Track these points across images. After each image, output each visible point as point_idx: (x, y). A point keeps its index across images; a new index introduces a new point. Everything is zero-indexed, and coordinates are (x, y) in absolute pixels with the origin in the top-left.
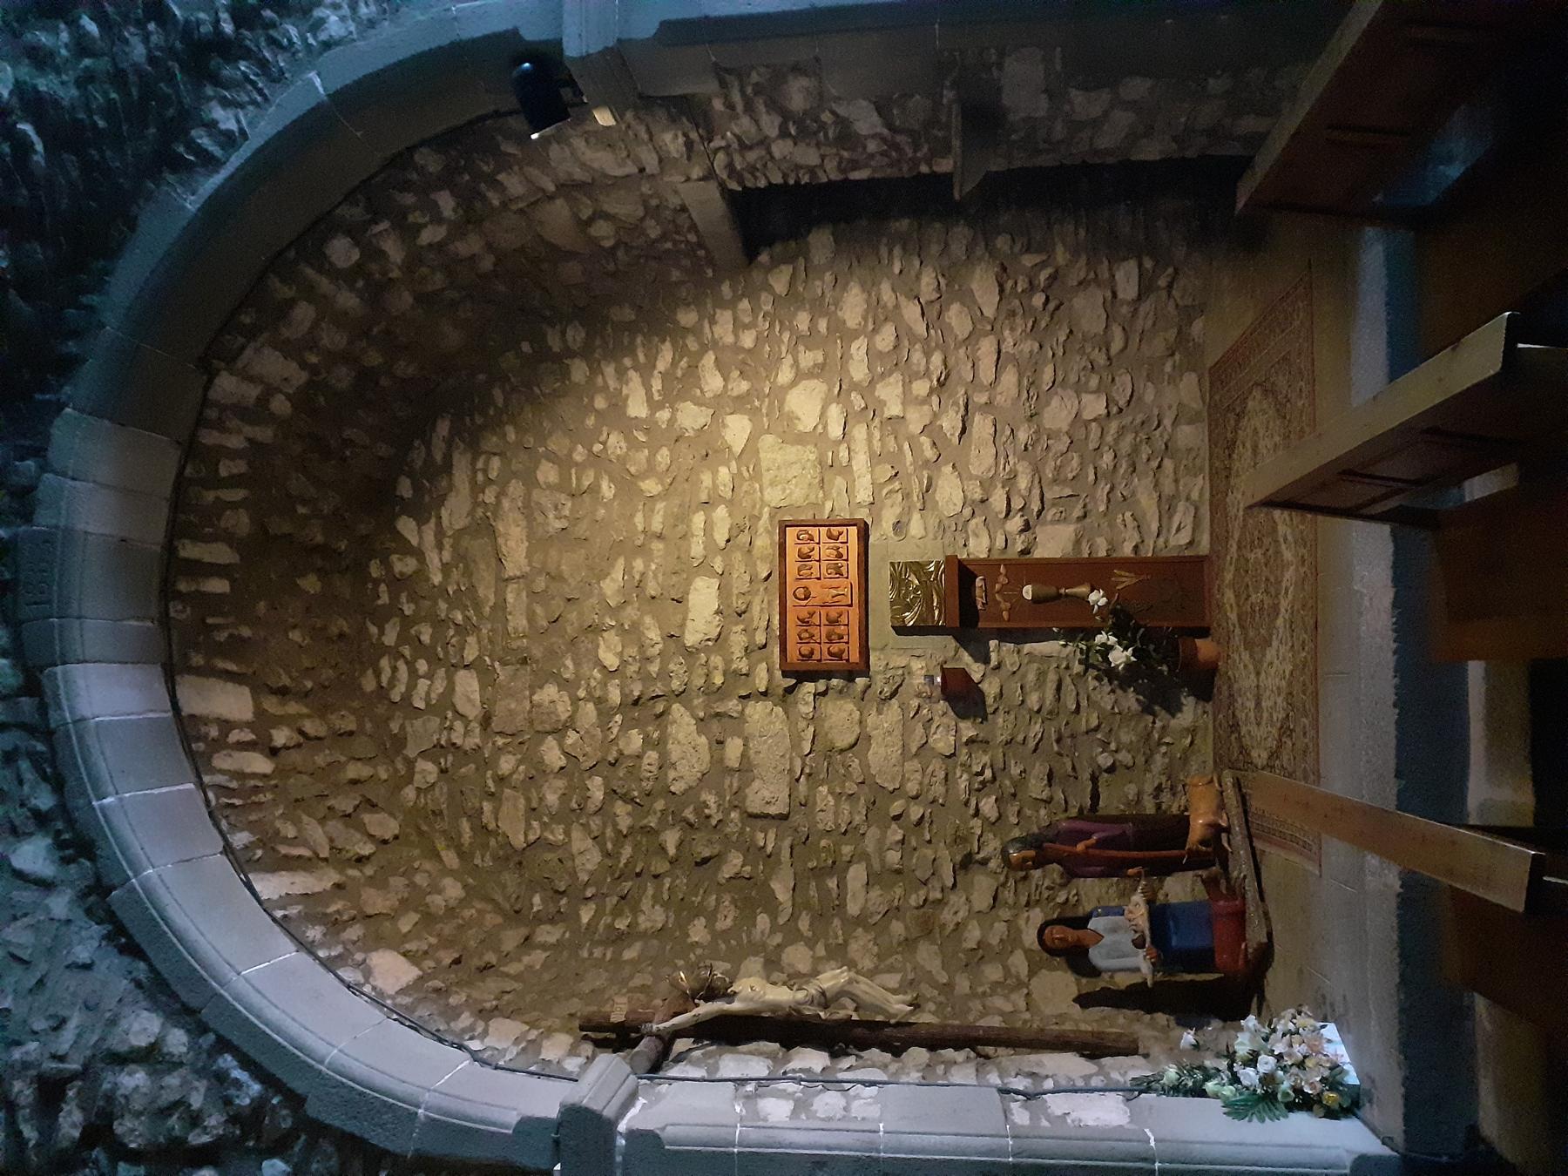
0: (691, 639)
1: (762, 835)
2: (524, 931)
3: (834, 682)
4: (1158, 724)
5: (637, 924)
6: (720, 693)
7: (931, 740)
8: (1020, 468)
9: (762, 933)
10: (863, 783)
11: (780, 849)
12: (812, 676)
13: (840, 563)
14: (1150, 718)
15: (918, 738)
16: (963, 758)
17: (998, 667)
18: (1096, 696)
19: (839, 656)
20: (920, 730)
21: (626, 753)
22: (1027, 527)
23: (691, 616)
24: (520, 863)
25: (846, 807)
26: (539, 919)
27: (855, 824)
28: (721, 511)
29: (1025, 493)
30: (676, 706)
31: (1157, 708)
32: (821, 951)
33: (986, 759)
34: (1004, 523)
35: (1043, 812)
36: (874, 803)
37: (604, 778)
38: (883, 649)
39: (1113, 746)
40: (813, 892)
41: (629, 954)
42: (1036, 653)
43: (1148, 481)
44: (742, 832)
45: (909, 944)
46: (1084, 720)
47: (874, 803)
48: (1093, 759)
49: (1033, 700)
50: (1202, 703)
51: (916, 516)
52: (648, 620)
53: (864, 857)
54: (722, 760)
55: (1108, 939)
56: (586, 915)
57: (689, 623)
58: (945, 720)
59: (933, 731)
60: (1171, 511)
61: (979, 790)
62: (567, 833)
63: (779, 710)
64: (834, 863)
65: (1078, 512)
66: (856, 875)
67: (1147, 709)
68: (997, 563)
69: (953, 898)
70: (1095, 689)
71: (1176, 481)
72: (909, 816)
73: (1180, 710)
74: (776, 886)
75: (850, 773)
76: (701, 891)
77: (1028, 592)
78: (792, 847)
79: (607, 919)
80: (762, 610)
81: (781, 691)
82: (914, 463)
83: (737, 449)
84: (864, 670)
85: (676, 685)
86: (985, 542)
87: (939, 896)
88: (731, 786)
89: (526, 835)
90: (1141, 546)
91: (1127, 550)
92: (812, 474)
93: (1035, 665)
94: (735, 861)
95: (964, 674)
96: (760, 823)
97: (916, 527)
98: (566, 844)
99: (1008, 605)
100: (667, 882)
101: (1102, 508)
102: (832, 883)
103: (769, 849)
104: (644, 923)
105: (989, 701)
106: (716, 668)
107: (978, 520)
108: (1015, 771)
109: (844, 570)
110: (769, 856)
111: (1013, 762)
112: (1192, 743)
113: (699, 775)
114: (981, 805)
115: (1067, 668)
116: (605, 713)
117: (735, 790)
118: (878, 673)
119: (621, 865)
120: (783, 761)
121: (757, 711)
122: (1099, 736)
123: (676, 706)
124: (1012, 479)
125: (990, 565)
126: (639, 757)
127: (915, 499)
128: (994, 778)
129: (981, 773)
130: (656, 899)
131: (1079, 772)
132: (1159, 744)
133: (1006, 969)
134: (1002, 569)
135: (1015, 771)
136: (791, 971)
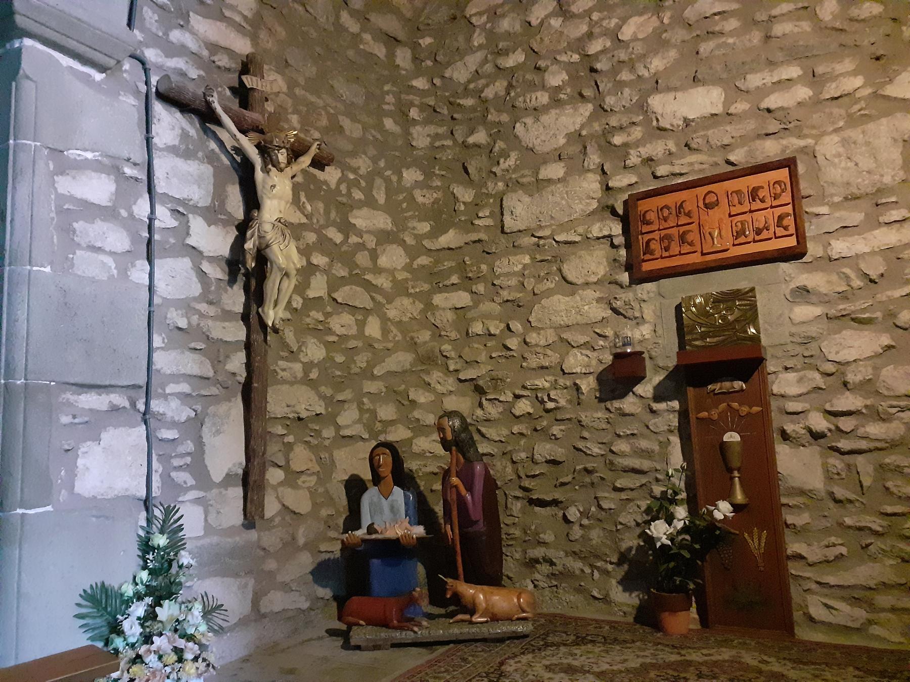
0: (656, 102)
1: (487, 214)
2: (401, 35)
3: (623, 252)
4: (610, 567)
5: (414, 126)
6: (607, 147)
7: (575, 350)
8: (895, 424)
9: (414, 228)
10: (534, 294)
11: (479, 231)
12: (626, 231)
13: (751, 235)
14: (615, 560)
15: (575, 339)
16: (561, 382)
17: (652, 411)
18: (632, 507)
19: (648, 250)
20: (582, 339)
21: (546, 74)
22: (817, 436)
23: (679, 95)
24: (455, 18)
25: (513, 282)
26: (415, 47)
27: (501, 292)
28: (803, 93)
29: (861, 431)
30: (590, 107)
31: (626, 567)
32: (401, 276)
33: (562, 402)
34: (818, 410)
35: (523, 455)
36: (519, 306)
37: (524, 63)
38: (660, 294)
39: (585, 522)
40: (448, 264)
41: (389, 123)
42: (670, 448)
43: (890, 577)
44: (488, 195)
45: (413, 345)
46: (606, 495)
47: (519, 306)
48: (573, 503)
49: (622, 446)
50: (634, 612)
51: (817, 311)
52: (673, 54)
53: (476, 304)
54: (545, 162)
55: (385, 504)
56: (420, 83)
57: (671, 95)
58: (594, 362)
59: (584, 352)
60: (855, 601)
61: (537, 397)
62: (481, 47)
63: (595, 205)
64: (470, 279)
65: (840, 493)
66: (462, 298)
67: (623, 558)
68: (766, 406)
69: (451, 380)
70: (638, 507)
71: (893, 610)
72: (510, 337)
73: (625, 590)
74: (451, 233)
75: (542, 281)
76: (443, 173)
77: (731, 437)
78: (479, 241)
79: (417, 100)
80: (691, 164)
81: (610, 203)
82: (891, 300)
83: (891, 91)
84: (638, 279)
85: (610, 101)
86: (793, 390)
87: (452, 368)
88: (523, 176)
89: (475, 15)
90: (803, 562)
91: (794, 546)
92: (864, 184)
93: (656, 448)
94: (467, 196)
95: (639, 378)
96: (497, 210)
97: (804, 312)
98: (471, 50)
99: (715, 417)
100: (449, 142)
101: (848, 521)
102: (454, 279)
103: (477, 222)
104: (416, 131)
105: (616, 404)
106: (629, 135)
107: (819, 380)
108: (556, 430)
109: (742, 239)
110: (472, 223)
111: (563, 427)
112: (594, 597)
113: (531, 145)
114: (524, 400)
115: (657, 480)
116: (579, 45)
117: (520, 180)
118: (635, 294)
119: (458, 101)
120: (548, 218)
121: (591, 184)
122: (593, 509)
123: (590, 107)
124: (882, 418)
125: (762, 396)
126: (544, 87)
127: (841, 307)
128: (548, 411)
129: (550, 399)
130: (437, 136)
131: (560, 489)
132: (592, 566)
133: (392, 423)
134: (756, 409)
135: (556, 430)
136: (378, 252)
